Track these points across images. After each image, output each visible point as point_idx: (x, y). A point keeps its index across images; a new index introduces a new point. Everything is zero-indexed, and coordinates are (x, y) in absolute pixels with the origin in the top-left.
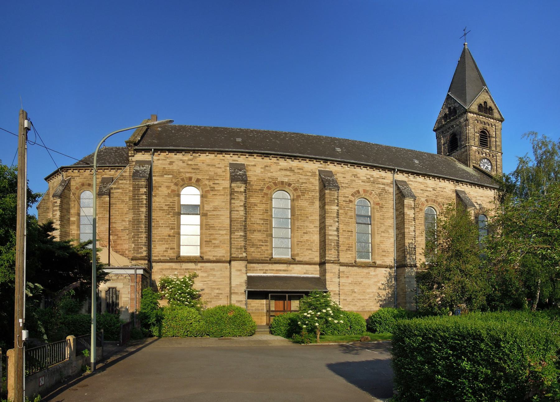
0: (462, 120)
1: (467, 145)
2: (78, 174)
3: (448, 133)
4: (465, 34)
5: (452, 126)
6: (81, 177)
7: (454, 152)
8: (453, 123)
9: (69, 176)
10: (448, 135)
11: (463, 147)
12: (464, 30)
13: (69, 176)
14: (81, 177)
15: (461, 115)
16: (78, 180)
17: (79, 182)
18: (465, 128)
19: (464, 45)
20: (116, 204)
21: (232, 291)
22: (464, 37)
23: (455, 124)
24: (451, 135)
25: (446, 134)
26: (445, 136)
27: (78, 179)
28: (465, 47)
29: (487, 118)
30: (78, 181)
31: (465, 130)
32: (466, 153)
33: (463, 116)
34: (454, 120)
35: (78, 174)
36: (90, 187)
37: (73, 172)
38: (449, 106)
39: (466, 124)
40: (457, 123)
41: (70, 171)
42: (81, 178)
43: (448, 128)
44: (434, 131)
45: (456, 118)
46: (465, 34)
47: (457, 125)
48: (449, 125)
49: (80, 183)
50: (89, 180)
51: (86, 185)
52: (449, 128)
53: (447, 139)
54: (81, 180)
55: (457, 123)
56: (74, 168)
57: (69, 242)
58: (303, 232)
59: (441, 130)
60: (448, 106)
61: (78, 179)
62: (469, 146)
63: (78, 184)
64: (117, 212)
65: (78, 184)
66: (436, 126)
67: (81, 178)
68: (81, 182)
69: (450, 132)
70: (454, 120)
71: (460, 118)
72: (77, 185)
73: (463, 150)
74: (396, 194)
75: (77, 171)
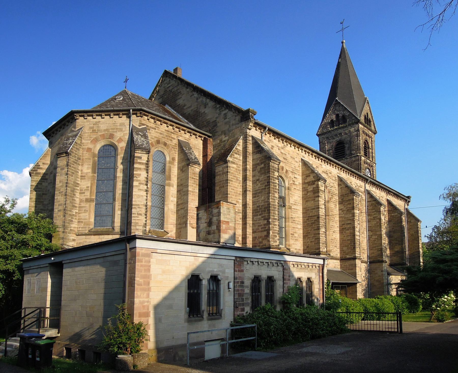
0: (352, 129)
1: (358, 154)
2: (154, 126)
3: (334, 140)
4: (343, 29)
5: (340, 134)
6: (157, 131)
7: (343, 160)
8: (340, 131)
9: (144, 125)
10: (334, 142)
11: (354, 156)
12: (341, 23)
13: (144, 125)
14: (157, 131)
15: (351, 125)
16: (153, 133)
17: (155, 137)
18: (356, 138)
19: (342, 43)
20: (232, 181)
21: (125, 250)
22: (341, 32)
23: (344, 132)
24: (337, 142)
25: (331, 141)
26: (330, 143)
27: (153, 132)
28: (343, 46)
29: (368, 130)
30: (154, 135)
31: (356, 140)
32: (358, 162)
33: (354, 126)
34: (343, 127)
35: (154, 126)
36: (166, 148)
37: (148, 119)
38: (336, 112)
39: (357, 134)
40: (346, 131)
41: (146, 118)
42: (157, 132)
43: (335, 135)
44: (317, 135)
45: (346, 127)
46: (343, 29)
47: (346, 134)
48: (336, 132)
49: (156, 139)
50: (164, 138)
51: (162, 143)
52: (336, 135)
53: (333, 145)
54: (157, 135)
55: (346, 131)
56: (153, 116)
57: (434, 263)
58: (333, 231)
59: (326, 136)
60: (335, 113)
61: (153, 132)
62: (360, 155)
63: (153, 139)
64: (233, 191)
65: (153, 139)
66: (319, 131)
67: (157, 132)
68: (157, 138)
69: (336, 139)
70: (343, 127)
71: (350, 127)
72: (153, 140)
73: (353, 159)
74: (368, 202)
75: (152, 121)
